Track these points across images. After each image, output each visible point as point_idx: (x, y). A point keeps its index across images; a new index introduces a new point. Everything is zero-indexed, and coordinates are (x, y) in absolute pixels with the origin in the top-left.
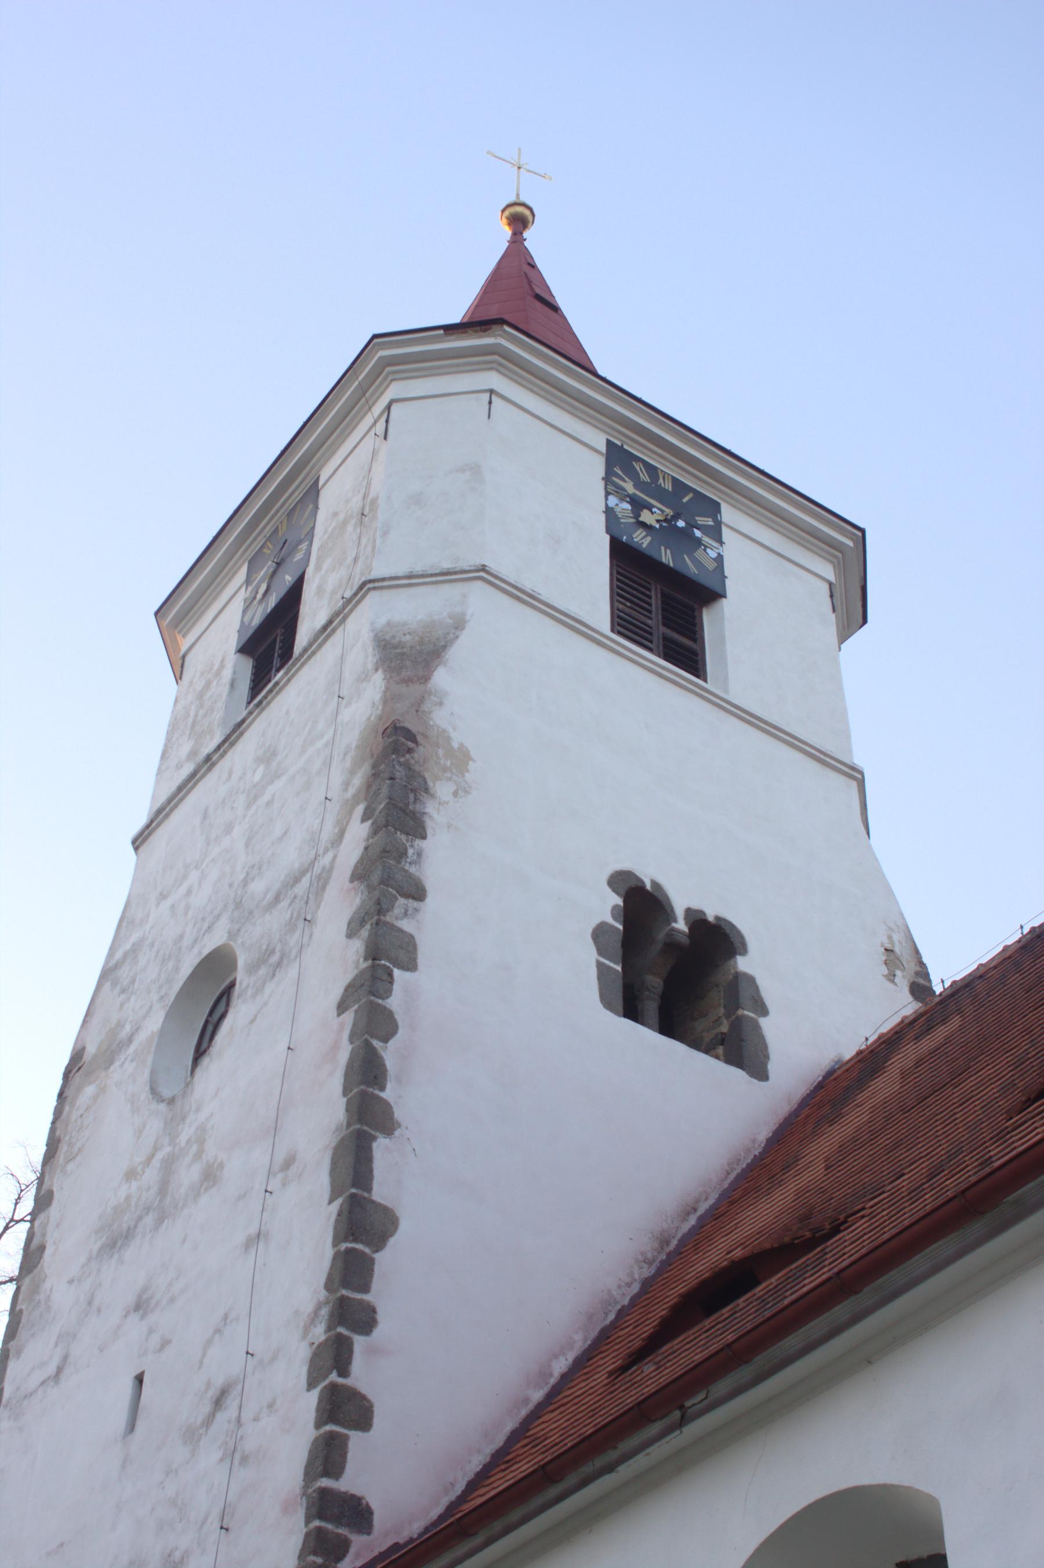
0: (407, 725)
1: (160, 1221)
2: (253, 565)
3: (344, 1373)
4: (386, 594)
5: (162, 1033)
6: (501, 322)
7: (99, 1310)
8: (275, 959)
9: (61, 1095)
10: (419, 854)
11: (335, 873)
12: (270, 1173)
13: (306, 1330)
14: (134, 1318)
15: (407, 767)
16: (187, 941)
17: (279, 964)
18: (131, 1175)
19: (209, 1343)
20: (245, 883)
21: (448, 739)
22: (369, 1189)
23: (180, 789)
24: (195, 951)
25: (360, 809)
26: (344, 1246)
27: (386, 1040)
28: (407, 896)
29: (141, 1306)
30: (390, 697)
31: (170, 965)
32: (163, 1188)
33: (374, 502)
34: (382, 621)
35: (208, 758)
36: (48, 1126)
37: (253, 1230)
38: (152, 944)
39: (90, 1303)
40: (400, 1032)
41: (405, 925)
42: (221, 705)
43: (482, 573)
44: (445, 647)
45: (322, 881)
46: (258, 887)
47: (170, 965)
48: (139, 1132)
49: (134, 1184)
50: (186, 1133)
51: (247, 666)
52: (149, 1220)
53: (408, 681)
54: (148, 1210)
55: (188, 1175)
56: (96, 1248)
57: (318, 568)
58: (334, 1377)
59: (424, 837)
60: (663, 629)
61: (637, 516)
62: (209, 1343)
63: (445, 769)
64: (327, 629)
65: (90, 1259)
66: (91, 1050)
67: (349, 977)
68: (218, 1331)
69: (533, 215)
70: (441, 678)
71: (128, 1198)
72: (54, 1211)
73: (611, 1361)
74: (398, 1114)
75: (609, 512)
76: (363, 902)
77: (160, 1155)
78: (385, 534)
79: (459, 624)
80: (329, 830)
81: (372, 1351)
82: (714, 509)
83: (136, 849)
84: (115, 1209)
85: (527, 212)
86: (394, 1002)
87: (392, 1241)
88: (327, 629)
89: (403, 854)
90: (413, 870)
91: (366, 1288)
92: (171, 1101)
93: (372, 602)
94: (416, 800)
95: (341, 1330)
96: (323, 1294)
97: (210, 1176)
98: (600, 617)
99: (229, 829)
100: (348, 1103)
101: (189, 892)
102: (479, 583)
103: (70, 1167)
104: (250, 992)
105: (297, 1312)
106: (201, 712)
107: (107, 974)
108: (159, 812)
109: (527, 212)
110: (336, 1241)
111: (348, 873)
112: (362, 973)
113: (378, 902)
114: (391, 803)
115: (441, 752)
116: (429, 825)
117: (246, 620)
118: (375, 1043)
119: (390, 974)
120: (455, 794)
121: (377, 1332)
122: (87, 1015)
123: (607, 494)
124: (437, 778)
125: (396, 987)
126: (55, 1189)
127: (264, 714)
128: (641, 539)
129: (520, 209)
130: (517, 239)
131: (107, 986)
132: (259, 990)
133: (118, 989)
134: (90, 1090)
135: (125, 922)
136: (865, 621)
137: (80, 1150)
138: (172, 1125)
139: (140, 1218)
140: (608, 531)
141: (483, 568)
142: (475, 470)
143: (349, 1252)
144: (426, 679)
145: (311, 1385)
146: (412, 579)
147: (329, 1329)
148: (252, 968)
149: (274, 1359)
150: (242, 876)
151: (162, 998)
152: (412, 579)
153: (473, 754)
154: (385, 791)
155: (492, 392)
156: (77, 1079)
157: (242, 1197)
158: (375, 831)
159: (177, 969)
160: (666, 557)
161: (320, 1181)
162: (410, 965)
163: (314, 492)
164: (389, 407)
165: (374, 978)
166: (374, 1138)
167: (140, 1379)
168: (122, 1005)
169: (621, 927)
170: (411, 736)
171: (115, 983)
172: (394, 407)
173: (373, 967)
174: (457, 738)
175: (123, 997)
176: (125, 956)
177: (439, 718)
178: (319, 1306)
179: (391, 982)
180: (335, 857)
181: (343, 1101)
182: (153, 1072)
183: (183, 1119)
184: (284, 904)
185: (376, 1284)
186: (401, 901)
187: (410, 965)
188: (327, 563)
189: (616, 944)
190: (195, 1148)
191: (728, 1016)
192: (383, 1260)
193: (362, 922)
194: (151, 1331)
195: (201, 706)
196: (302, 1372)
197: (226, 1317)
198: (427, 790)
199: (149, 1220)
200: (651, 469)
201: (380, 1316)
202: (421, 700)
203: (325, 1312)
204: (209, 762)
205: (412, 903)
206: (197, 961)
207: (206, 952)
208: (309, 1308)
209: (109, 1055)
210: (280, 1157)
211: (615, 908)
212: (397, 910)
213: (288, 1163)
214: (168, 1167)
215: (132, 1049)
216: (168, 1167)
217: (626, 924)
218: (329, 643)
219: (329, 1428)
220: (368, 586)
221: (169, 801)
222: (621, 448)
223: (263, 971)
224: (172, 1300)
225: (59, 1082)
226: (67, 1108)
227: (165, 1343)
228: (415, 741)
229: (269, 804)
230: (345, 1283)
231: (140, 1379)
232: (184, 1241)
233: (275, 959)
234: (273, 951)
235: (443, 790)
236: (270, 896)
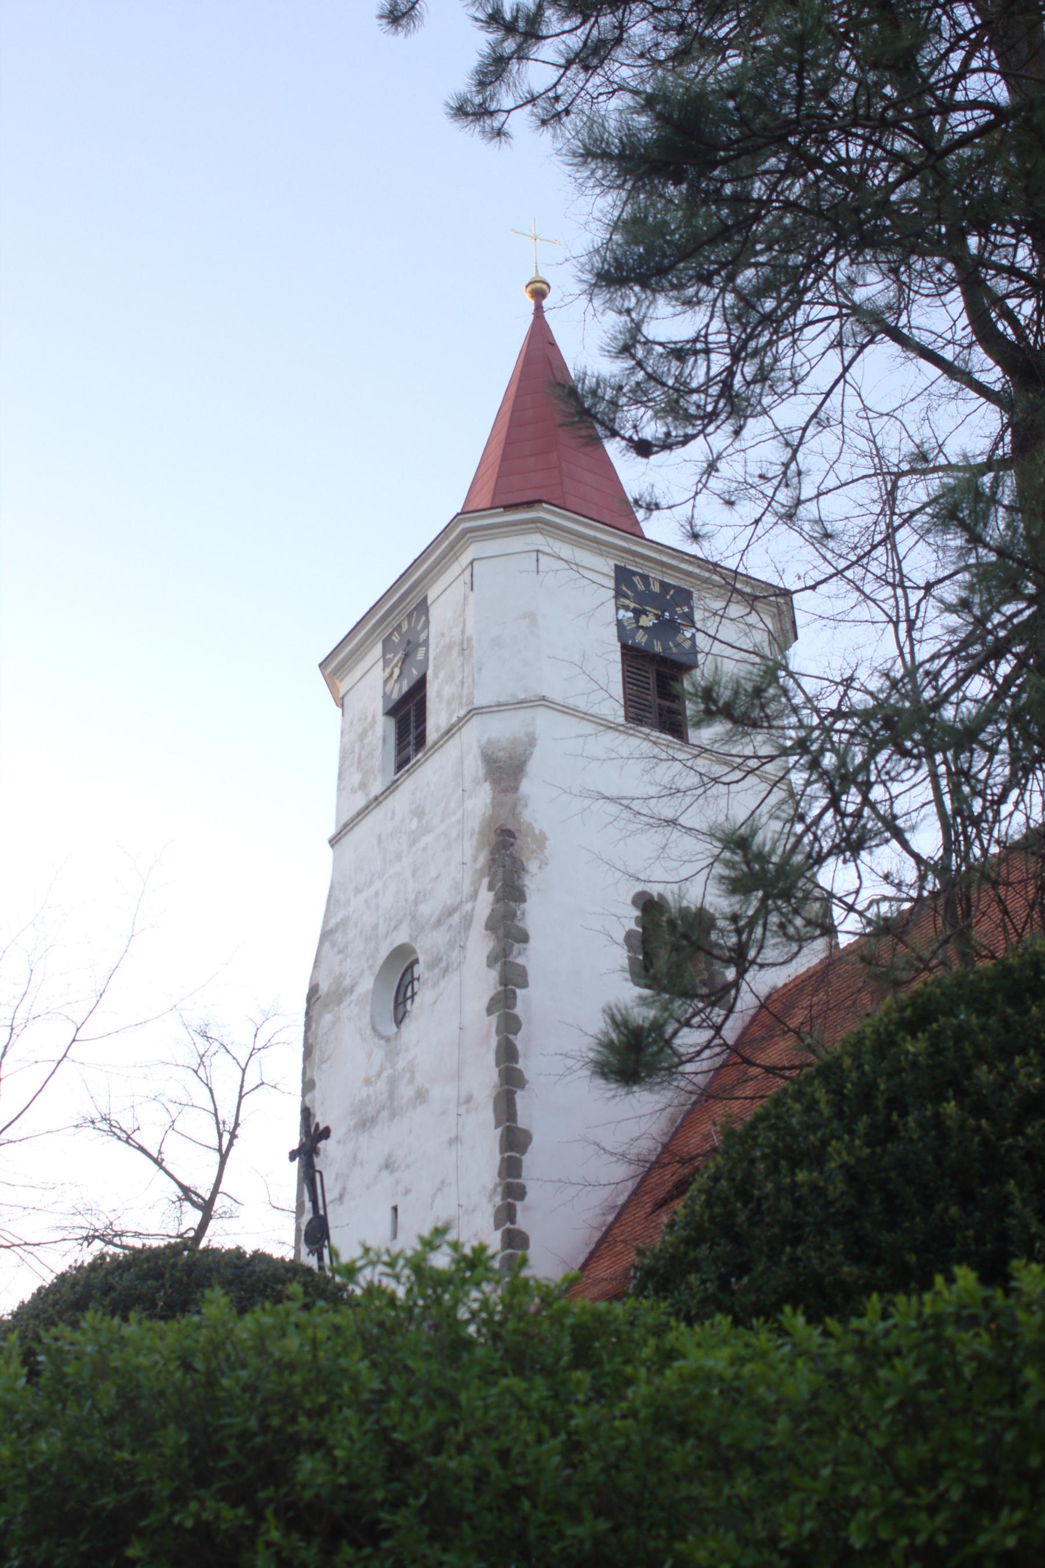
0: (509, 827)
1: (393, 1115)
2: (387, 643)
3: (513, 1222)
4: (486, 718)
5: (374, 991)
6: (540, 501)
7: (362, 1164)
8: (443, 964)
9: (307, 1014)
10: (523, 913)
11: (475, 919)
12: (459, 1104)
13: (491, 1198)
14: (385, 1173)
15: (511, 856)
16: (382, 931)
17: (446, 970)
18: (368, 1082)
19: (434, 1196)
20: (416, 903)
21: (533, 829)
22: (515, 1121)
23: (359, 814)
24: (389, 940)
25: (486, 881)
26: (506, 1155)
27: (516, 1034)
28: (518, 942)
29: (388, 1165)
30: (496, 804)
31: (372, 945)
32: (391, 1096)
33: (469, 640)
34: (485, 738)
35: (376, 798)
36: (302, 1034)
37: (453, 1135)
38: (356, 924)
39: (355, 1158)
40: (523, 1027)
41: (520, 961)
42: (378, 753)
43: (543, 701)
44: (525, 762)
45: (467, 921)
46: (425, 909)
47: (372, 945)
48: (369, 1055)
49: (371, 1090)
50: (401, 1064)
51: (392, 724)
52: (385, 1114)
53: (505, 791)
54: (383, 1108)
55: (406, 1092)
56: (352, 1123)
57: (436, 675)
58: (508, 1225)
59: (524, 901)
60: (659, 701)
61: (637, 621)
62: (434, 1196)
63: (533, 852)
64: (449, 733)
65: (349, 1131)
66: (324, 988)
67: (491, 993)
68: (439, 1189)
69: (549, 287)
70: (526, 786)
71: (368, 1096)
72: (317, 1092)
73: (648, 1200)
74: (526, 1075)
75: (619, 623)
76: (494, 949)
77: (386, 1074)
78: (480, 669)
79: (532, 742)
80: (467, 888)
81: (526, 1209)
82: (688, 595)
83: (332, 846)
84: (361, 1101)
85: (544, 287)
86: (518, 1010)
87: (530, 1148)
88: (449, 733)
89: (514, 915)
90: (520, 924)
91: (519, 1176)
92: (388, 1040)
93: (475, 722)
94: (519, 877)
95: (510, 1200)
96: (497, 1180)
97: (421, 1096)
98: (614, 709)
99: (399, 858)
100: (500, 1072)
101: (377, 895)
102: (541, 709)
103: (324, 1066)
104: (430, 983)
105: (484, 1187)
106: (364, 753)
107: (326, 935)
108: (345, 826)
109: (544, 287)
110: (502, 1151)
111: (483, 923)
112: (498, 993)
113: (504, 950)
114: (505, 884)
115: (529, 840)
116: (527, 891)
117: (388, 689)
118: (511, 1037)
119: (514, 993)
120: (540, 867)
121: (527, 1198)
122: (316, 961)
123: (617, 609)
124: (529, 859)
125: (519, 1001)
126: (316, 1079)
127: (411, 778)
128: (641, 638)
129: (539, 285)
130: (539, 311)
131: (327, 945)
132: (436, 984)
133: (336, 949)
134: (327, 1018)
135: (332, 902)
136: (796, 638)
137: (329, 1057)
138: (392, 1054)
139: (379, 1112)
140: (620, 639)
141: (544, 698)
142: (531, 616)
143: (509, 1157)
144: (516, 789)
145: (497, 1228)
146: (500, 707)
147: (503, 1199)
148: (432, 965)
149: (474, 1210)
150: (413, 897)
151: (370, 967)
152: (500, 707)
153: (548, 835)
154: (500, 875)
155: (538, 551)
156: (317, 1007)
157: (443, 1113)
158: (498, 900)
159: (377, 949)
160: (658, 648)
161: (487, 1115)
162: (524, 985)
163: (423, 607)
164: (472, 563)
165: (507, 998)
166: (515, 1092)
167: (395, 1209)
168: (341, 962)
169: (640, 930)
170: (510, 834)
171: (333, 944)
172: (475, 564)
173: (505, 991)
174: (538, 826)
175: (340, 956)
176: (337, 925)
177: (527, 815)
178: (496, 1186)
179: (515, 997)
180: (473, 909)
181: (496, 1071)
182: (372, 1017)
183: (398, 1053)
184: (444, 928)
185: (524, 1173)
186: (517, 946)
187: (524, 985)
188: (442, 675)
189: (637, 943)
190: (408, 1076)
191: (707, 969)
192: (527, 1159)
193: (496, 960)
194: (397, 1182)
195: (362, 748)
196: (490, 1220)
197: (443, 1182)
198: (523, 869)
199: (385, 1114)
200: (645, 578)
201: (528, 1190)
202: (515, 807)
203: (500, 1189)
204: (377, 801)
205: (522, 946)
206: (391, 949)
207: (396, 944)
208: (490, 1186)
209: (340, 994)
210: (464, 1095)
211: (637, 918)
212: (515, 952)
213: (469, 1100)
214: (393, 1081)
215: (354, 996)
216: (393, 1081)
217: (644, 928)
218: (451, 742)
219: (509, 1251)
220: (473, 712)
221: (352, 820)
222: (625, 568)
223: (436, 971)
224: (408, 1166)
225: (304, 1005)
226: (314, 1026)
227: (407, 1191)
228: (514, 837)
229: (425, 849)
230: (509, 1175)
231: (395, 1209)
232: (410, 1132)
233: (443, 964)
234: (441, 960)
235: (532, 866)
236: (434, 919)
